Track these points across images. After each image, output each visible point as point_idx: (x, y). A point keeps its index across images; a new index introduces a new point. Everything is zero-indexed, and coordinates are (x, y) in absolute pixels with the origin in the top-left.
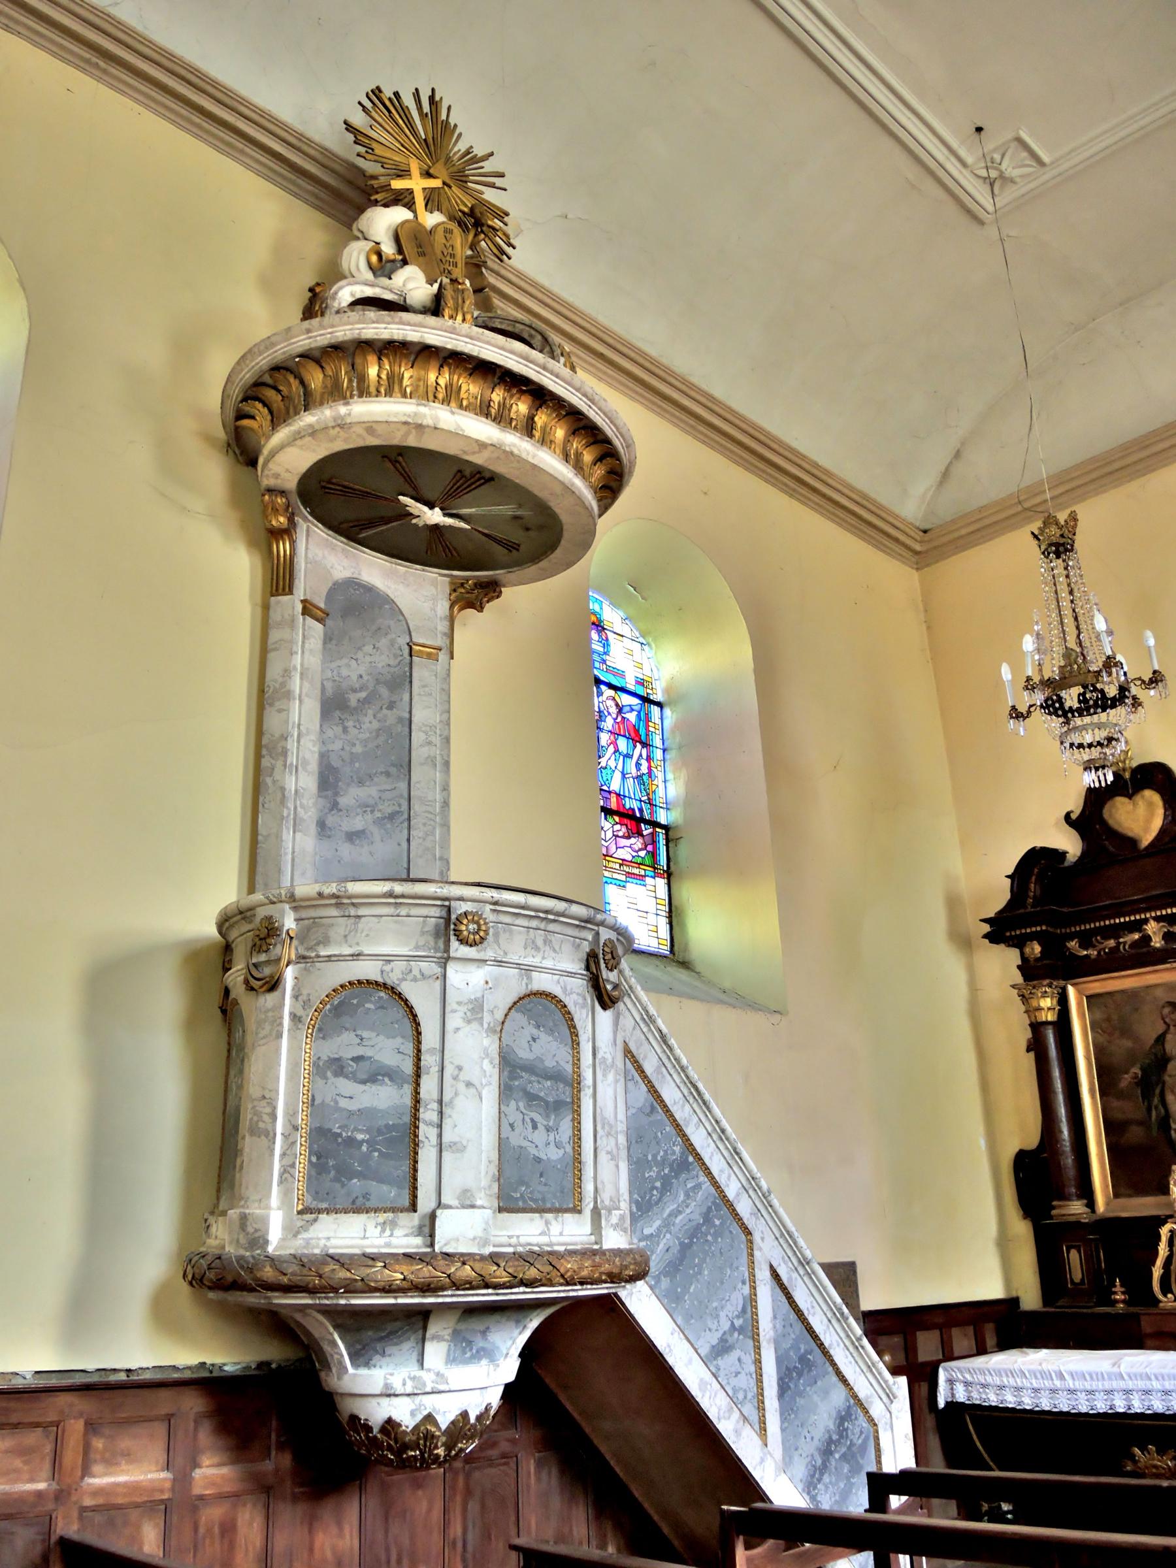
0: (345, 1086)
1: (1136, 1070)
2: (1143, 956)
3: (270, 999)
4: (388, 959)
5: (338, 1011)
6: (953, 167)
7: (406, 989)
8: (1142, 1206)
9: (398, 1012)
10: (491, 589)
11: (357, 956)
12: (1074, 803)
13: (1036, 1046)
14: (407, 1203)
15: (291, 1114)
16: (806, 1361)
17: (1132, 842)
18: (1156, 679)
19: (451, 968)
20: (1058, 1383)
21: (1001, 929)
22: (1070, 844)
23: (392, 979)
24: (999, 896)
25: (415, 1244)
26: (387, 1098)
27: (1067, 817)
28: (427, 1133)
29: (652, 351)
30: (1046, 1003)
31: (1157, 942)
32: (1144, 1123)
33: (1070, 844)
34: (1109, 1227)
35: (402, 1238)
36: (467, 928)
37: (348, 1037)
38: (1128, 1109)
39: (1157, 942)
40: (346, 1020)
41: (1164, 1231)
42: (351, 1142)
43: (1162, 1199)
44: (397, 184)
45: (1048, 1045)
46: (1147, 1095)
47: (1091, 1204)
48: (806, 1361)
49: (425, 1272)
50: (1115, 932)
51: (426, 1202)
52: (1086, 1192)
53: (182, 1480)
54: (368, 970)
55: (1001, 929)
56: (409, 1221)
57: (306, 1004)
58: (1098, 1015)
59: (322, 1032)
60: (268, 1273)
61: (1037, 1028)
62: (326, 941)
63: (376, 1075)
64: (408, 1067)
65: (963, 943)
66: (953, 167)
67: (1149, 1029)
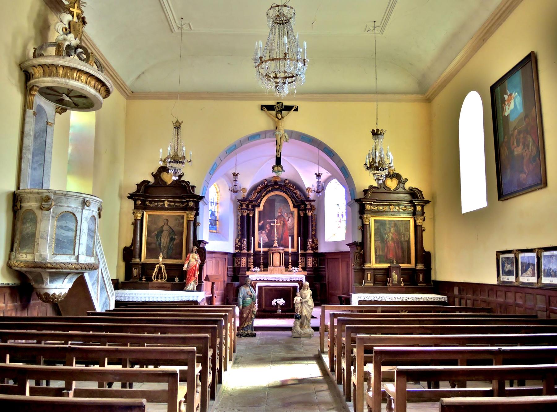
0: (63, 231)
1: (156, 232)
2: (163, 208)
3: (47, 212)
4: (73, 208)
5: (62, 216)
6: (173, 22)
7: (76, 214)
8: (152, 261)
9: (74, 218)
10: (64, 110)
11: (68, 206)
12: (155, 171)
13: (135, 224)
14: (72, 253)
15: (51, 236)
16: (104, 287)
17: (166, 183)
18: (190, 161)
19: (84, 211)
20: (134, 296)
21: (132, 197)
22: (151, 180)
23: (74, 212)
24: (134, 189)
25: (75, 261)
26: (71, 234)
27: (152, 173)
28: (77, 241)
29: (91, 37)
30: (140, 215)
31: (166, 206)
32: (155, 244)
33: (151, 180)
34: (144, 265)
35: (72, 260)
36: (88, 203)
37: (64, 222)
38: (151, 240)
39: (166, 206)
40: (64, 218)
41: (156, 266)
42: (64, 242)
43: (156, 260)
44: (71, 9)
45: (137, 224)
46: (157, 238)
47: (141, 260)
48: (104, 287)
49: (78, 266)
50: (158, 201)
51: (76, 254)
52: (140, 257)
53: (7, 306)
54: (69, 209)
55: (132, 197)
56: (74, 257)
57: (56, 214)
58: (150, 219)
59: (59, 220)
60: (49, 265)
61: (136, 220)
62: (61, 202)
63: (69, 230)
64: (74, 229)
65: (121, 197)
66: (173, 22)
67: (161, 224)
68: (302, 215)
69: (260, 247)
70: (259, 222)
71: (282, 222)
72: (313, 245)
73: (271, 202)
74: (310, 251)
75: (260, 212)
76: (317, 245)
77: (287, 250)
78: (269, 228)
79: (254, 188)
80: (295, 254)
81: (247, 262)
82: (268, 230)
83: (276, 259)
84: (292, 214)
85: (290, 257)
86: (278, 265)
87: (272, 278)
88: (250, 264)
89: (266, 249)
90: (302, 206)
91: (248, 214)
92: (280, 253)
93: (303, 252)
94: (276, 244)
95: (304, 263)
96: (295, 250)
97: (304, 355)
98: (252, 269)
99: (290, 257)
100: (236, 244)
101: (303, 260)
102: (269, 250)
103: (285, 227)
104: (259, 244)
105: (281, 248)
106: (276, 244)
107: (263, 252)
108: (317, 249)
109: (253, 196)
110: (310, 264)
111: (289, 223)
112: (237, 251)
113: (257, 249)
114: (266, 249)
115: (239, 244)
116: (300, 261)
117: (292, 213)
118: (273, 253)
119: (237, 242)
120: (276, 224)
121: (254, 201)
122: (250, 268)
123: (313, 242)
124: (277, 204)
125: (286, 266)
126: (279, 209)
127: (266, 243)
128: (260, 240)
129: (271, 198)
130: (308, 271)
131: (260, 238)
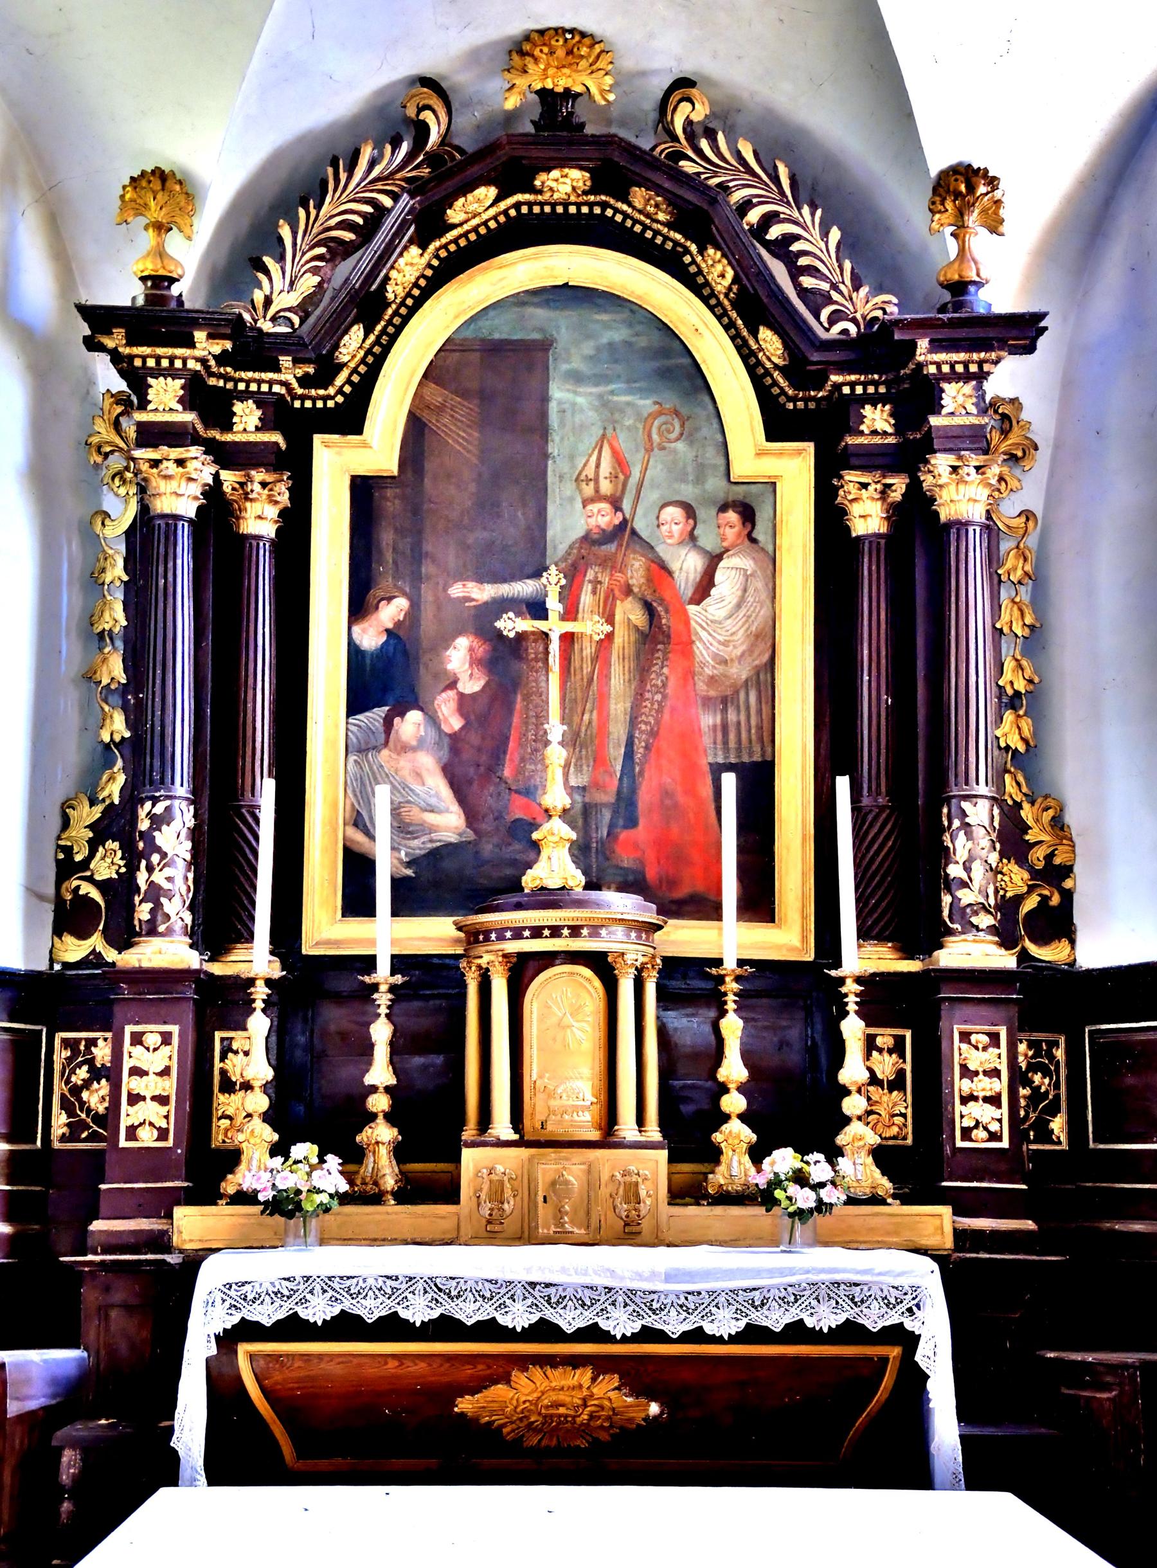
68: (867, 516)
69: (357, 900)
70: (360, 606)
71: (630, 613)
72: (1017, 878)
73: (495, 374)
74: (971, 951)
75: (364, 491)
76: (1055, 874)
77: (686, 938)
78: (472, 684)
79: (295, 187)
80: (796, 993)
81: (201, 1085)
82: (464, 701)
83: (564, 1047)
84: (748, 514)
85: (732, 1027)
86: (585, 1125)
87: (500, 1290)
88: (225, 1103)
89: (434, 933)
90: (877, 419)
91: (217, 509)
92: (602, 966)
93: (882, 960)
94: (554, 867)
95: (901, 1103)
96: (787, 938)
97: (386, 537)
98: (258, 1172)
99: (732, 1027)
100: (67, 867)
101: (885, 1066)
102: (475, 937)
103: (665, 673)
104: (357, 871)
105: (624, 904)
106: (554, 867)
107: (399, 963)
108: (1057, 923)
109: (284, 291)
110: (980, 1116)
111: (716, 628)
112: (74, 950)
113: (325, 928)
114: (434, 933)
115: (107, 865)
116: (852, 1071)
117: (748, 508)
118: (522, 971)
119: (80, 834)
120: (555, 626)
121: (290, 344)
122: (232, 1158)
123: (1012, 840)
124: (570, 402)
125: (688, 1130)
126: (591, 441)
127: (437, 855)
128: (360, 821)
129: (502, 329)
130: (963, 1204)
131: (365, 788)
